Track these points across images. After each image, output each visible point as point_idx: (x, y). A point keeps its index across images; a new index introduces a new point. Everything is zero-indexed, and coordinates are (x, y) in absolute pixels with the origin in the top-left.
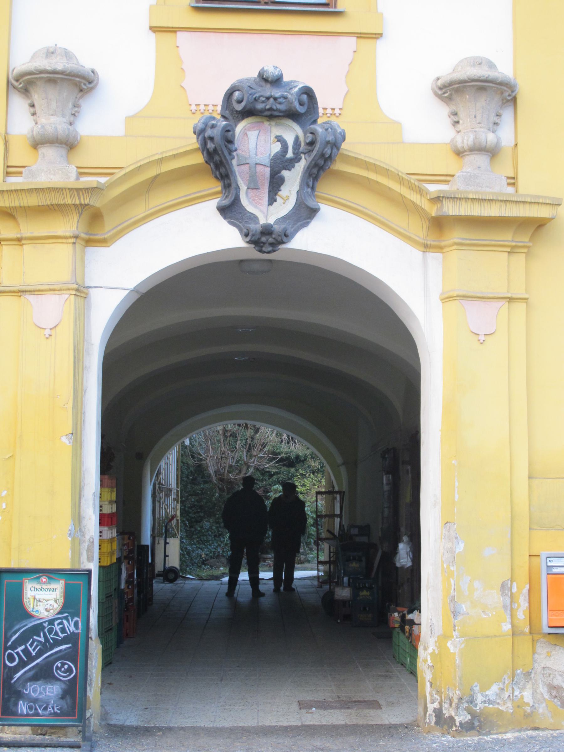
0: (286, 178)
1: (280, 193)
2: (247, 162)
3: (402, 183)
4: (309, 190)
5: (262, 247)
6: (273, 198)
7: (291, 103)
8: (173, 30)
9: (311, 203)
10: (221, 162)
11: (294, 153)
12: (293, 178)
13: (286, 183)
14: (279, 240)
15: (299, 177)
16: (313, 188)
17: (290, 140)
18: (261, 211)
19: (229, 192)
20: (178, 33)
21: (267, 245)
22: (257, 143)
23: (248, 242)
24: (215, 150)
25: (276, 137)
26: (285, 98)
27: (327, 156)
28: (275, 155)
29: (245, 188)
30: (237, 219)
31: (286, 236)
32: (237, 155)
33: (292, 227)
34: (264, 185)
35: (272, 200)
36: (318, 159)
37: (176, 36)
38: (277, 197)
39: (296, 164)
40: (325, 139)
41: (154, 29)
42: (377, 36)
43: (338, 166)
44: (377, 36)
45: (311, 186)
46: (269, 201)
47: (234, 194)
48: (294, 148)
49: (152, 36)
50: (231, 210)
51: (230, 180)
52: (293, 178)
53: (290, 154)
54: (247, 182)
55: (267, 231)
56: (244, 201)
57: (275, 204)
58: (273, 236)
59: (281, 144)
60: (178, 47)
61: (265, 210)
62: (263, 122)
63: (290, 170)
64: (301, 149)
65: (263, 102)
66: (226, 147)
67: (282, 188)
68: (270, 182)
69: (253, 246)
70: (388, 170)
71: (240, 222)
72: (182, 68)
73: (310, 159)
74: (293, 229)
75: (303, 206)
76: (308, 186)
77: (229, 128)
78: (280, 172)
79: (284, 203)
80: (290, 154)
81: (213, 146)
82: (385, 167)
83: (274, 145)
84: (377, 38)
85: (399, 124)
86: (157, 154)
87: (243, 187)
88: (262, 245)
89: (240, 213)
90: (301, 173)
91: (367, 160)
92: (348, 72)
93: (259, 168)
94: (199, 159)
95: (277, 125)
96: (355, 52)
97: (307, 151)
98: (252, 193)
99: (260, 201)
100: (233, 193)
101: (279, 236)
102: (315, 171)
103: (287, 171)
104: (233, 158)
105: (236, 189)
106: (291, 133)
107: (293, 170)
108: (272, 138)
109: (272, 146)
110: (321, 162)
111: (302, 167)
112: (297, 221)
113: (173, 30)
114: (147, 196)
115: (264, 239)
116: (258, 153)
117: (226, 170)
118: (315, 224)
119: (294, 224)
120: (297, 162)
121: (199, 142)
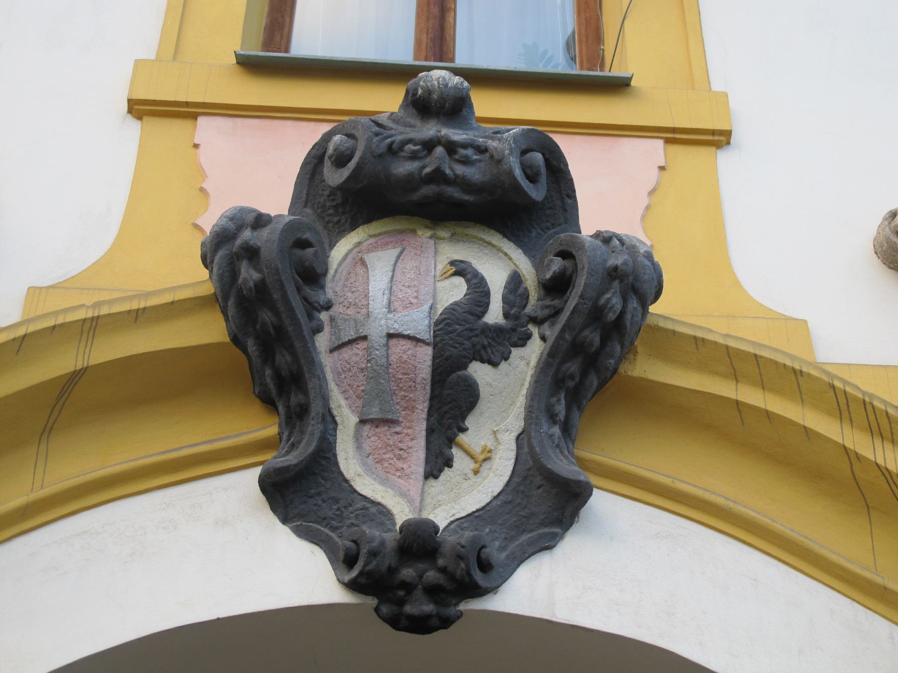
0: (483, 391)
1: (462, 438)
2: (363, 332)
3: (845, 414)
4: (556, 430)
5: (401, 603)
6: (441, 454)
7: (499, 162)
8: (187, 112)
9: (564, 467)
10: (280, 330)
11: (506, 315)
12: (506, 391)
13: (482, 405)
14: (458, 573)
15: (524, 391)
16: (567, 429)
17: (496, 277)
18: (403, 495)
19: (302, 432)
20: (201, 120)
21: (418, 593)
22: (393, 287)
23: (352, 586)
24: (261, 288)
25: (452, 263)
26: (482, 150)
27: (612, 316)
28: (451, 310)
29: (354, 419)
30: (323, 521)
31: (485, 566)
32: (332, 319)
33: (502, 548)
34: (413, 409)
35: (437, 463)
36: (582, 329)
37: (195, 127)
38: (455, 451)
39: (515, 352)
40: (605, 261)
41: (138, 108)
42: (716, 138)
43: (645, 367)
44: (716, 138)
45: (562, 416)
46: (427, 461)
47: (317, 435)
48: (505, 300)
49: (134, 127)
50: (300, 491)
51: (306, 393)
52: (506, 391)
53: (495, 315)
54: (359, 403)
55: (419, 541)
56: (349, 462)
57: (447, 473)
58: (441, 562)
59: (468, 281)
60: (196, 146)
61: (415, 492)
62: (413, 232)
63: (495, 364)
64: (529, 309)
65: (414, 156)
66: (299, 290)
67: (469, 422)
68: (432, 398)
69: (372, 601)
70: (798, 373)
71: (334, 529)
72: (202, 190)
73: (552, 332)
74: (503, 555)
75: (538, 480)
76: (552, 418)
77: (307, 235)
78: (465, 367)
79: (476, 472)
80: (495, 315)
81: (256, 276)
82: (789, 363)
83: (447, 283)
84: (718, 145)
85: (805, 322)
86: (82, 306)
87: (347, 418)
88: (401, 593)
89: (336, 500)
90: (528, 379)
91: (732, 343)
92: (648, 208)
93: (399, 348)
94: (211, 330)
95: (454, 238)
96: (662, 168)
97: (546, 312)
98: (373, 437)
99: (400, 464)
100: (312, 434)
101: (460, 557)
102: (573, 367)
103: (486, 368)
104: (319, 329)
105: (324, 418)
106: (499, 265)
107: (503, 365)
108: (440, 267)
109: (439, 284)
110: (593, 337)
111: (533, 361)
112: (520, 528)
113: (187, 112)
114: (43, 447)
115: (408, 573)
116: (396, 304)
117: (294, 354)
118: (573, 546)
119: (509, 539)
120: (516, 345)
121: (214, 277)
